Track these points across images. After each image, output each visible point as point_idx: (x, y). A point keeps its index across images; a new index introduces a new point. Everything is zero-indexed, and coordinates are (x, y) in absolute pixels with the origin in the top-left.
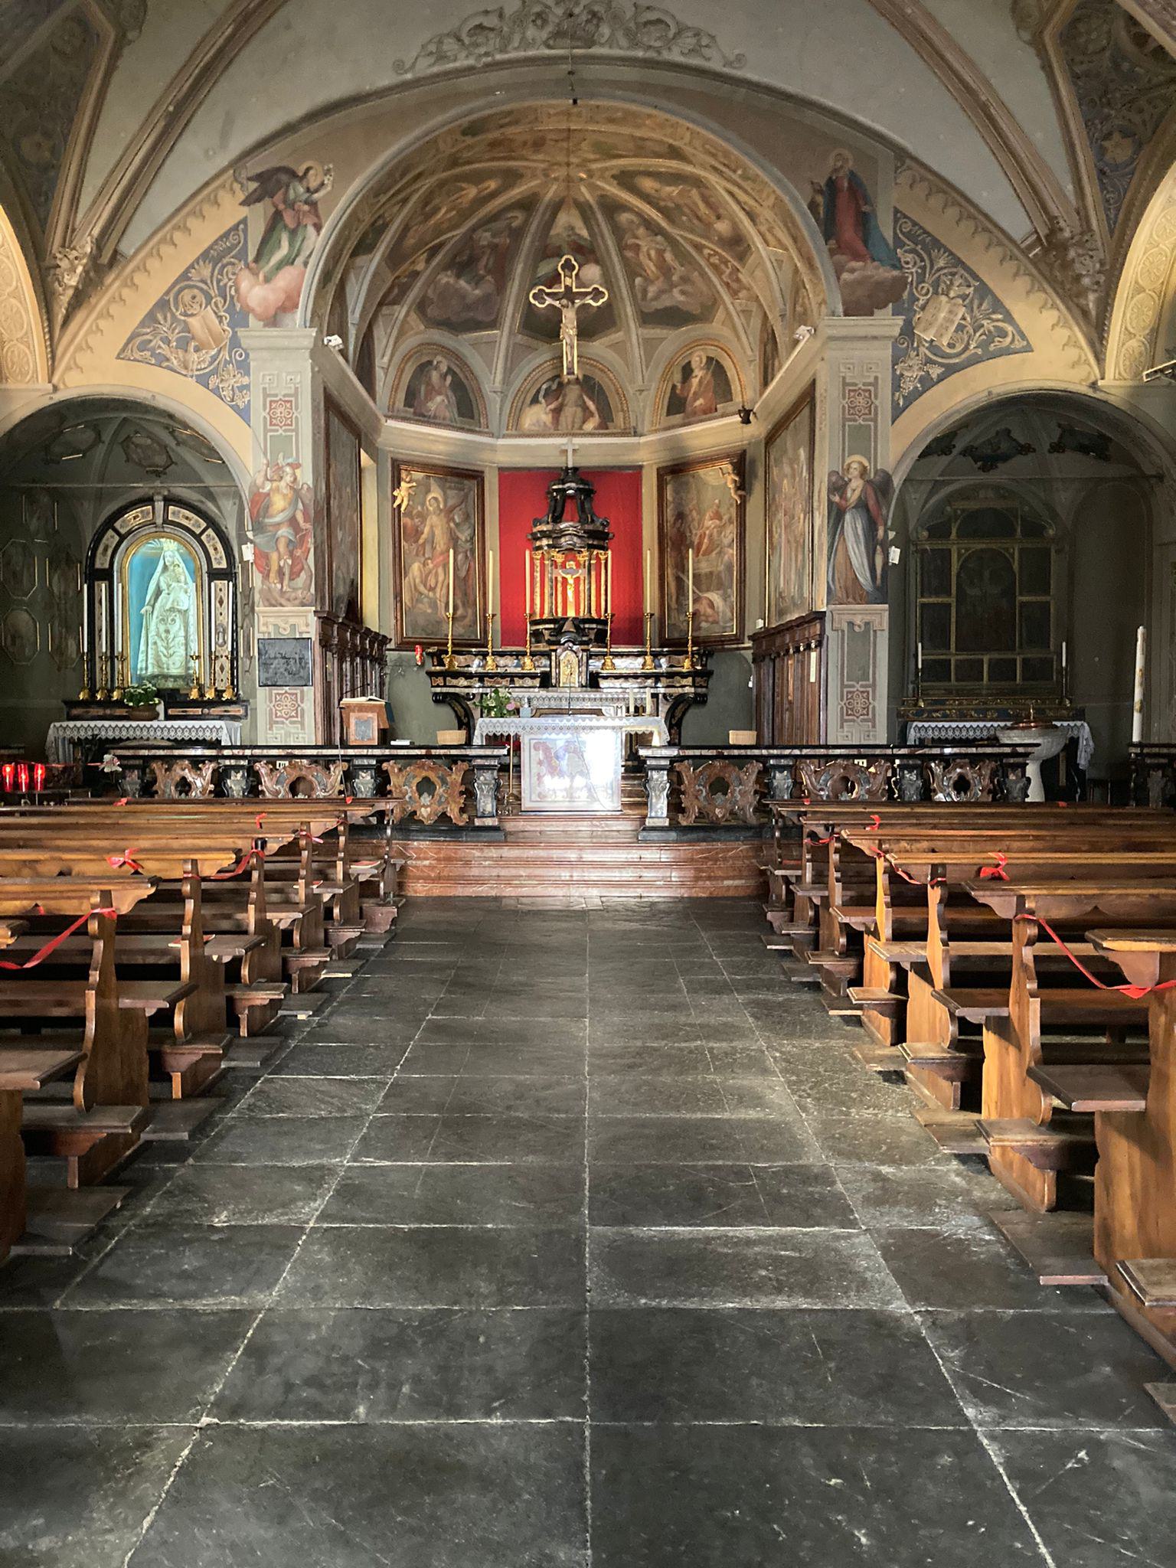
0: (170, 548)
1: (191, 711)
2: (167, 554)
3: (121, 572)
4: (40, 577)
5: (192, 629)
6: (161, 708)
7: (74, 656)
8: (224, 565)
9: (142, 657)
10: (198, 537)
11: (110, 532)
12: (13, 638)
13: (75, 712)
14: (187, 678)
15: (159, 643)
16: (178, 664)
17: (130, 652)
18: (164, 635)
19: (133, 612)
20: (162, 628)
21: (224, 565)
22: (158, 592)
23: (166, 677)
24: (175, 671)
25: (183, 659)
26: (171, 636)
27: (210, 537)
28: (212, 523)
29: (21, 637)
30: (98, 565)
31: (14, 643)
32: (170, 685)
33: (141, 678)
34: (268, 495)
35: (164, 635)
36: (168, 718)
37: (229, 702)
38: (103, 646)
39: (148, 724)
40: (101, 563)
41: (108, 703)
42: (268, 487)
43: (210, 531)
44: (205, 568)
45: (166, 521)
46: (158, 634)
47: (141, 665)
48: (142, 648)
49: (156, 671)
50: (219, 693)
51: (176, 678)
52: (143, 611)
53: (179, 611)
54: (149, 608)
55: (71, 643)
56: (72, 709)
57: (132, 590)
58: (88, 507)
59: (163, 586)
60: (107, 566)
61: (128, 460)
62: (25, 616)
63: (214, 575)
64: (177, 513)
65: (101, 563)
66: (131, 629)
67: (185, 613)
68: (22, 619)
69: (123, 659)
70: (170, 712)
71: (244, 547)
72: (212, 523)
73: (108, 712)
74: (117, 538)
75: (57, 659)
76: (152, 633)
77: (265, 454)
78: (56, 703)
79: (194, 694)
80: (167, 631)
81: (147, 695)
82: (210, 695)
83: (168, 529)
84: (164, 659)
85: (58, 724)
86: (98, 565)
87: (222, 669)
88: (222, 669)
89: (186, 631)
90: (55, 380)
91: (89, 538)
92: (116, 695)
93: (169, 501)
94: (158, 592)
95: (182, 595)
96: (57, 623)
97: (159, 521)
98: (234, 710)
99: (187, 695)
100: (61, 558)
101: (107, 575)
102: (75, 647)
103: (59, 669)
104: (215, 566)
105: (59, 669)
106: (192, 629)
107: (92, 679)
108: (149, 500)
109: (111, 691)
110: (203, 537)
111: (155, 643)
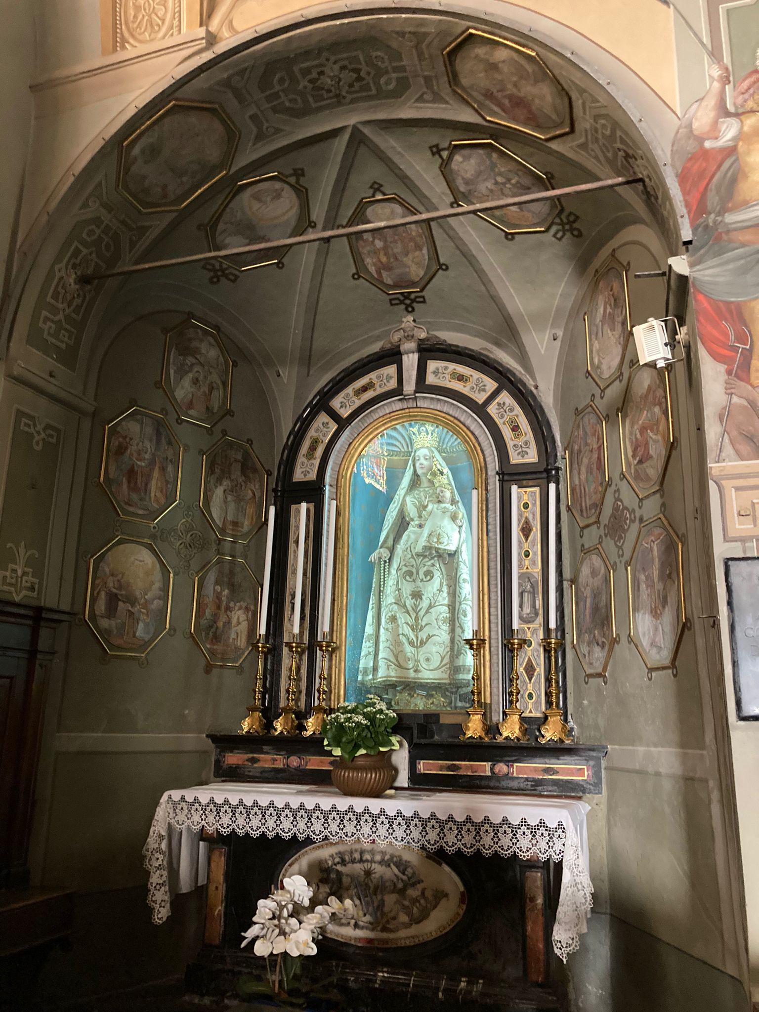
0: (427, 442)
1: (466, 767)
2: (422, 453)
3: (337, 486)
4: (181, 489)
5: (467, 590)
6: (401, 757)
7: (242, 642)
8: (532, 456)
9: (367, 646)
10: (480, 410)
11: (323, 417)
12: (113, 600)
13: (233, 759)
14: (449, 689)
15: (402, 618)
16: (436, 661)
17: (345, 637)
18: (409, 603)
19: (354, 560)
20: (407, 588)
21: (532, 456)
22: (402, 524)
23: (410, 687)
24: (430, 673)
25: (443, 650)
26: (425, 604)
27: (506, 409)
28: (506, 380)
29: (131, 600)
30: (298, 476)
31: (112, 610)
32: (419, 704)
33: (363, 690)
34: (731, 151)
35: (409, 603)
36: (421, 783)
37: (557, 750)
38: (294, 625)
39: (375, 805)
40: (304, 470)
41: (295, 743)
42: (729, 131)
43: (505, 397)
44: (494, 465)
45: (421, 385)
46: (399, 602)
47: (365, 662)
48: (369, 629)
49: (393, 674)
50: (532, 726)
51: (431, 689)
52: (374, 557)
53: (440, 556)
54: (385, 554)
55: (239, 616)
56: (231, 756)
57: (356, 520)
58: (288, 375)
59: (411, 511)
60: (313, 476)
61: (356, 276)
62: (146, 558)
63: (511, 475)
64: (440, 372)
65: (304, 470)
66: (351, 595)
67: (450, 559)
68: (138, 564)
69: (332, 650)
70: (422, 766)
71: (639, 331)
72: (506, 380)
73: (294, 761)
74: (334, 427)
75: (205, 647)
76: (389, 599)
77: (715, 54)
78: (194, 740)
79: (474, 728)
80: (417, 595)
81: (375, 732)
82: (511, 730)
83: (426, 402)
84: (409, 649)
85: (176, 794)
86: (298, 476)
87: (530, 670)
88: (530, 670)
89: (454, 594)
90: (214, 25)
91: (286, 425)
92: (312, 725)
93: (429, 350)
94: (402, 524)
95: (447, 525)
96: (212, 577)
97: (409, 387)
98: (567, 769)
99: (459, 729)
100: (229, 459)
101: (313, 492)
102: (244, 626)
103: (208, 668)
104: (515, 459)
105: (208, 668)
106: (467, 590)
107: (271, 690)
108: (393, 356)
109: (302, 716)
110: (492, 410)
111: (393, 619)
